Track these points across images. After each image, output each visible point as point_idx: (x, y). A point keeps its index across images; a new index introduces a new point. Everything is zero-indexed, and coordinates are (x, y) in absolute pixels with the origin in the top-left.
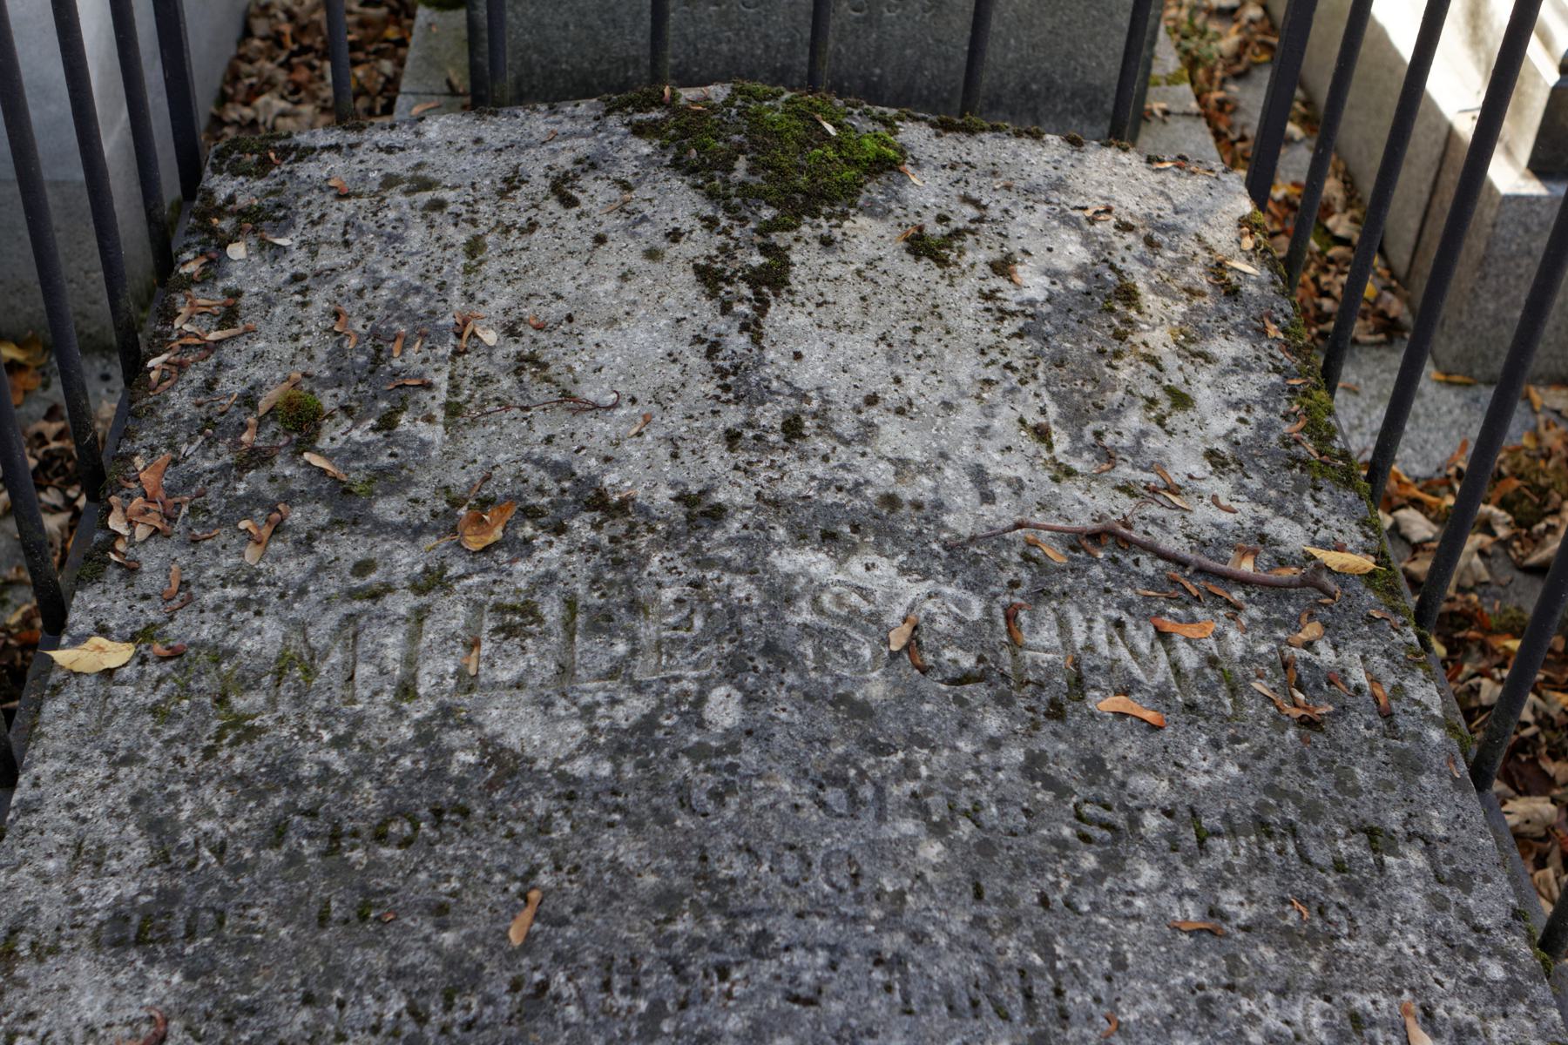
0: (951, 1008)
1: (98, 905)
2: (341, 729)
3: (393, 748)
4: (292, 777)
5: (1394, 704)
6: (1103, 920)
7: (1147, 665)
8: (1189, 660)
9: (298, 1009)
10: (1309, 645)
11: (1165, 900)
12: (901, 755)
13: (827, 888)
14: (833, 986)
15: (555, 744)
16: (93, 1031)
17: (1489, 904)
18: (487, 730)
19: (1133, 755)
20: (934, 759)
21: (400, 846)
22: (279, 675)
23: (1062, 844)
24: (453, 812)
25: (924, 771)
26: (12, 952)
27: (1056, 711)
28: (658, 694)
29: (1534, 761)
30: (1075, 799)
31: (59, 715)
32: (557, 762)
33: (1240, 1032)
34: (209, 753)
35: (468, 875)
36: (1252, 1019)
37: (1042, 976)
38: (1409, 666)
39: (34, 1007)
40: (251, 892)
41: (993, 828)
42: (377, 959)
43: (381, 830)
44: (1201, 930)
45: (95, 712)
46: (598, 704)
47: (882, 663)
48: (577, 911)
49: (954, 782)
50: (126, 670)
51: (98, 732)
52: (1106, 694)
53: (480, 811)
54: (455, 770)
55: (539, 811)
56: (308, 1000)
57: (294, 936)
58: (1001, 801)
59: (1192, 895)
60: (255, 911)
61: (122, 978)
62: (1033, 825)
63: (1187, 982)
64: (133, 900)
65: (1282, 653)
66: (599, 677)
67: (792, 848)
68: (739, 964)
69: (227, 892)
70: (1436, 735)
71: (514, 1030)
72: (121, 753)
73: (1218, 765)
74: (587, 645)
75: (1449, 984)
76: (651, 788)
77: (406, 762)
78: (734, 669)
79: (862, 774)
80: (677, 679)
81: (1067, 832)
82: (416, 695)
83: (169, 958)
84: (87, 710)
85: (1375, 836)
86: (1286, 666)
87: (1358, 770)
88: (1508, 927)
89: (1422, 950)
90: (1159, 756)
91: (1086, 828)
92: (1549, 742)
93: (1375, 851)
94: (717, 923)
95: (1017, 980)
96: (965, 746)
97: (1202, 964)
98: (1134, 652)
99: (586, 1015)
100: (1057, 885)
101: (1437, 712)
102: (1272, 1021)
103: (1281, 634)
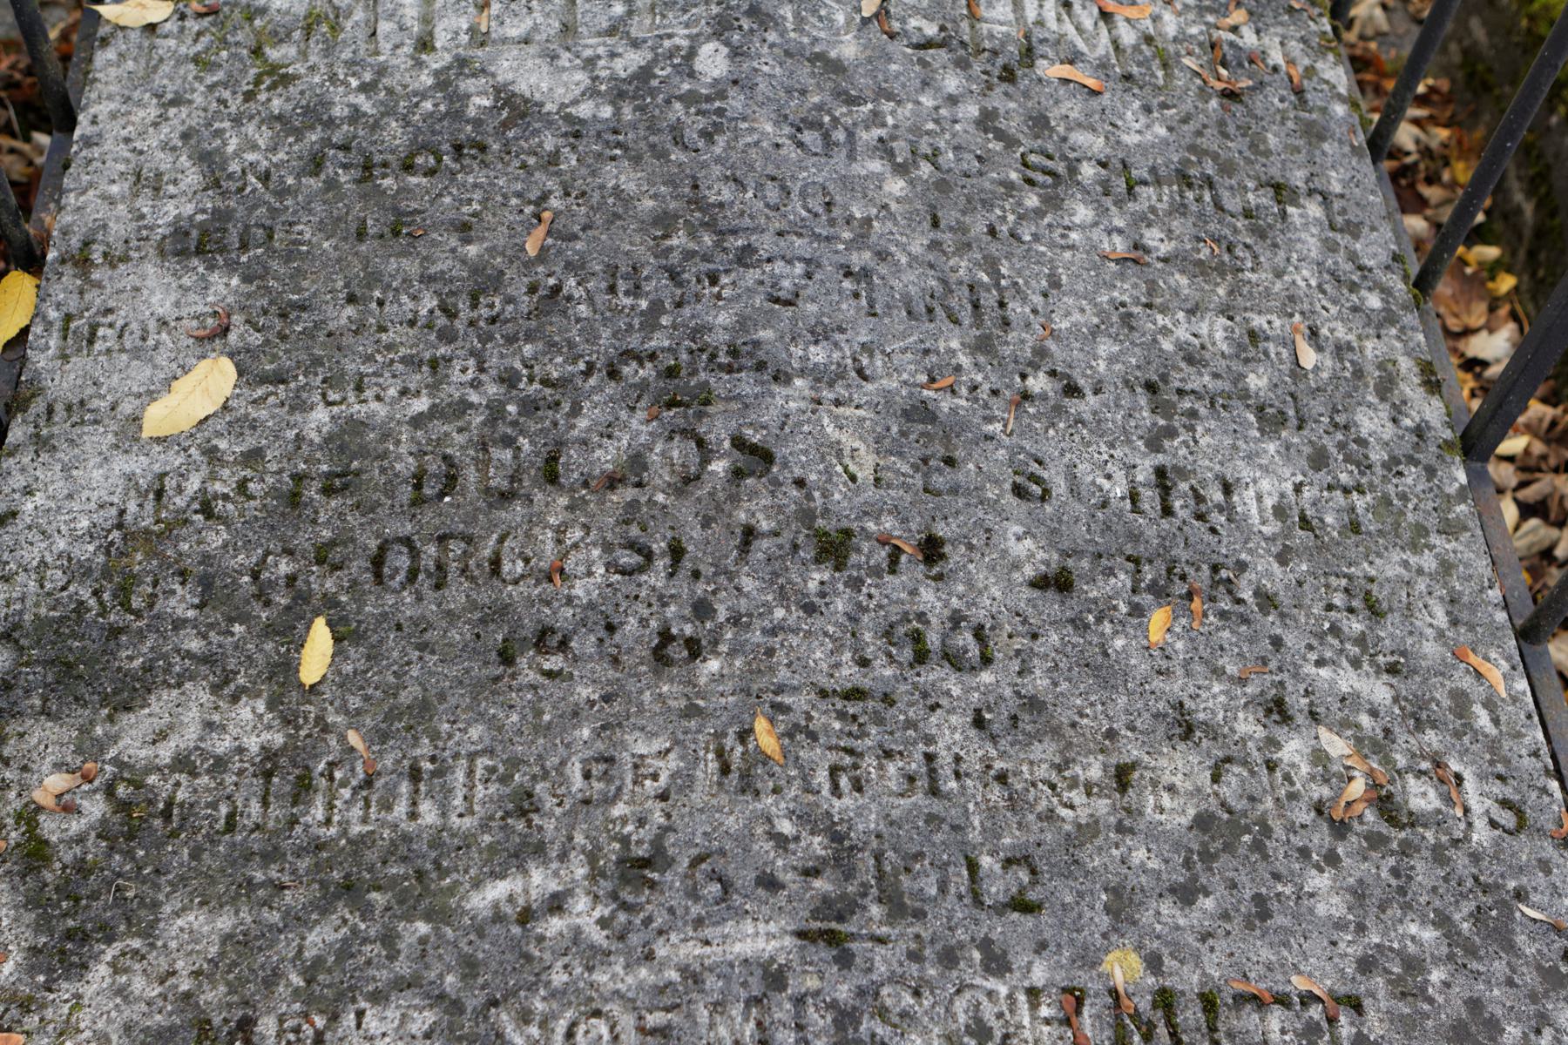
0: (909, 313)
1: (160, 222)
2: (368, 77)
3: (415, 94)
4: (325, 117)
5: (1305, 82)
6: (1042, 249)
7: (1090, 41)
8: (1128, 37)
9: (343, 307)
10: (1234, 29)
11: (1096, 234)
12: (870, 106)
13: (804, 213)
14: (809, 291)
15: (561, 91)
16: (165, 323)
17: (1374, 249)
18: (499, 79)
19: (1074, 115)
20: (899, 110)
21: (425, 175)
22: (308, 31)
23: (1009, 186)
24: (472, 147)
25: (890, 121)
26: (87, 260)
27: (1008, 75)
28: (653, 49)
29: (1412, 186)
30: (1022, 149)
31: (109, 63)
32: (563, 106)
33: (1155, 340)
34: (249, 96)
35: (487, 199)
36: (1165, 331)
37: (988, 290)
38: (1323, 51)
39: (111, 304)
40: (295, 212)
41: (949, 170)
42: (411, 267)
43: (408, 162)
44: (1126, 259)
45: (143, 62)
46: (599, 57)
47: (854, 28)
48: (584, 229)
49: (917, 130)
50: (168, 26)
51: (147, 78)
52: (1053, 62)
53: (496, 147)
54: (472, 112)
55: (549, 146)
56: (351, 299)
57: (336, 248)
58: (957, 148)
59: (1120, 231)
60: (301, 227)
61: (186, 281)
62: (984, 169)
63: (1112, 301)
64: (191, 218)
65: (1210, 35)
66: (599, 34)
67: (773, 179)
68: (727, 272)
69: (274, 213)
70: (1340, 110)
71: (533, 324)
72: (169, 96)
73: (1148, 127)
74: (587, 6)
75: (1334, 310)
76: (648, 128)
77: (428, 105)
78: (721, 28)
79: (835, 120)
80: (670, 36)
81: (1014, 176)
82: (433, 49)
83: (226, 264)
84: (135, 59)
85: (1280, 190)
86: (1213, 46)
87: (1270, 136)
88: (1387, 267)
89: (1313, 283)
90: (1097, 117)
91: (1030, 174)
92: (1427, 168)
93: (1279, 202)
94: (708, 239)
95: (966, 292)
96: (927, 101)
97: (1126, 286)
98: (1079, 29)
99: (595, 312)
100: (1004, 218)
101: (1342, 90)
102: (1182, 333)
103: (1210, 18)
